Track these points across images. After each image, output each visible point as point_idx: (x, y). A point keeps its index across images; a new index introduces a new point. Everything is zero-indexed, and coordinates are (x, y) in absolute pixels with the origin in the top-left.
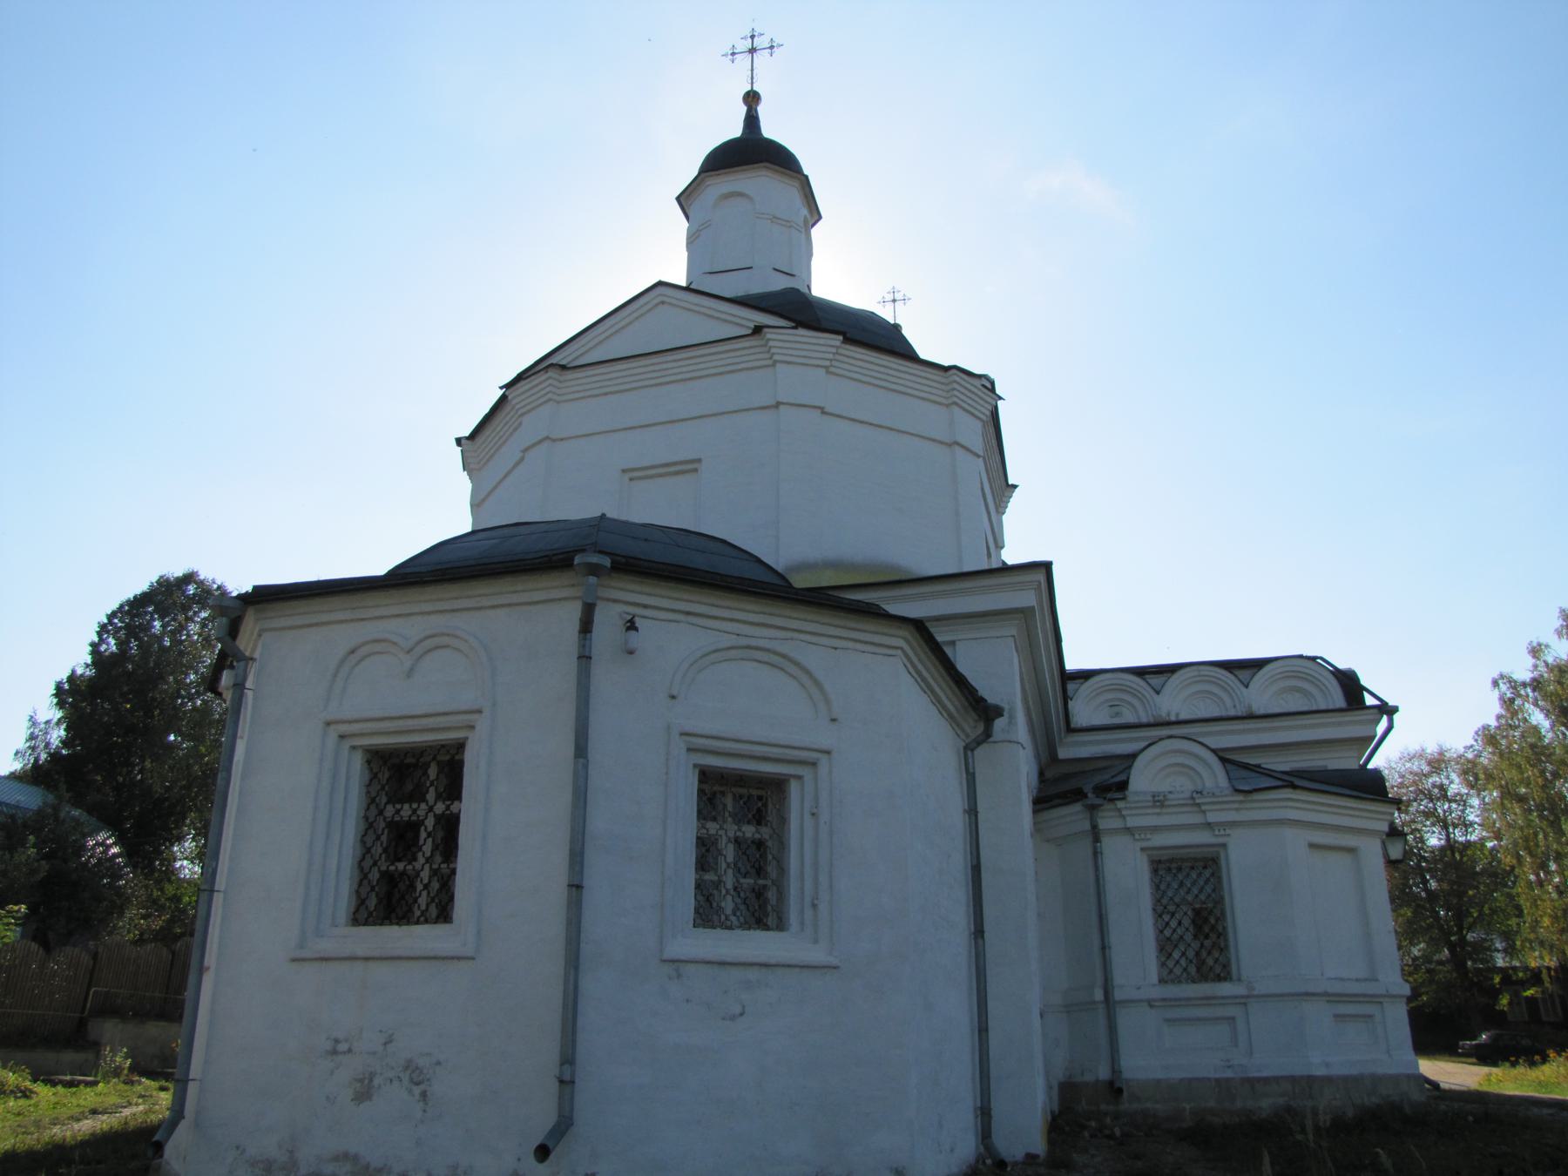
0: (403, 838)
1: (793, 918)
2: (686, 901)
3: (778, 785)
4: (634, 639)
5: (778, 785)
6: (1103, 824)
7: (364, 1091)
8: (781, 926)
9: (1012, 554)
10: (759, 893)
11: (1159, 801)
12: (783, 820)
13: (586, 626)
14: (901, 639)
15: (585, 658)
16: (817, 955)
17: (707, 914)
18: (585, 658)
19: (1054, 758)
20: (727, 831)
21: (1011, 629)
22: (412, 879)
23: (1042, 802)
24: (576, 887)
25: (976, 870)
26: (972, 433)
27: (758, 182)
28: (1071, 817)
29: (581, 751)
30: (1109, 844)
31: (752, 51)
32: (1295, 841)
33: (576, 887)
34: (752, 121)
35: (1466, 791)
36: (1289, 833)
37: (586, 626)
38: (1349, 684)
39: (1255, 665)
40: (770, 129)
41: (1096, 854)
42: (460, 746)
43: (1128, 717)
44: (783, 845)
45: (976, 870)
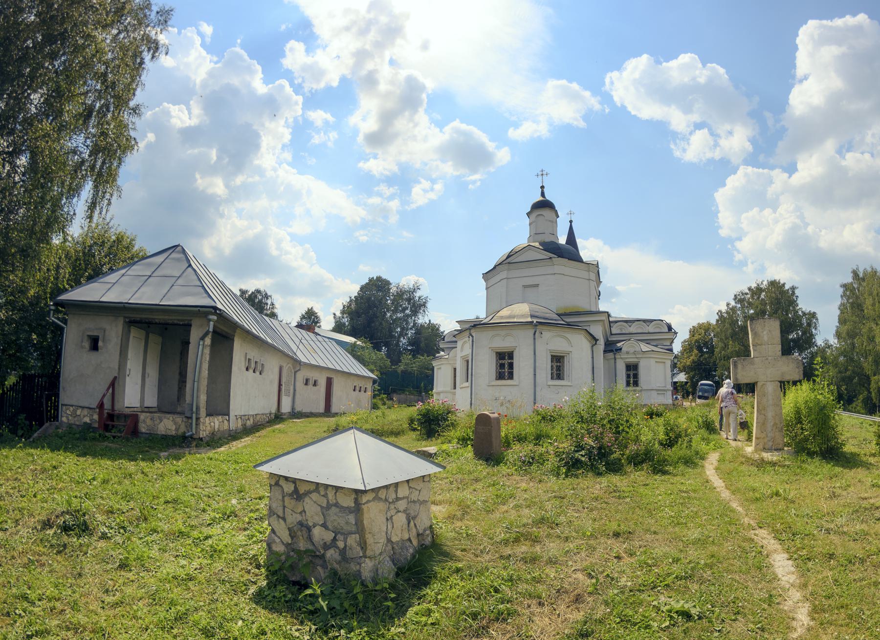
0: (502, 366)
1: (565, 378)
2: (550, 376)
3: (563, 357)
4: (542, 335)
5: (563, 357)
6: (617, 357)
7: (502, 405)
8: (563, 379)
9: (602, 309)
10: (560, 374)
11: (628, 353)
12: (564, 362)
13: (535, 334)
14: (583, 332)
15: (534, 339)
16: (569, 384)
17: (552, 378)
18: (534, 339)
19: (608, 340)
20: (555, 364)
21: (601, 323)
22: (504, 372)
23: (605, 352)
24: (535, 375)
25: (593, 368)
26: (593, 276)
27: (546, 212)
28: (611, 355)
29: (535, 354)
30: (617, 360)
31: (542, 175)
32: (653, 361)
33: (535, 375)
34: (543, 194)
35: (262, 562)
36: (652, 359)
37: (535, 334)
38: (670, 328)
39: (651, 321)
40: (549, 197)
41: (615, 362)
42: (513, 352)
43: (624, 332)
44: (563, 366)
45: (593, 368)
